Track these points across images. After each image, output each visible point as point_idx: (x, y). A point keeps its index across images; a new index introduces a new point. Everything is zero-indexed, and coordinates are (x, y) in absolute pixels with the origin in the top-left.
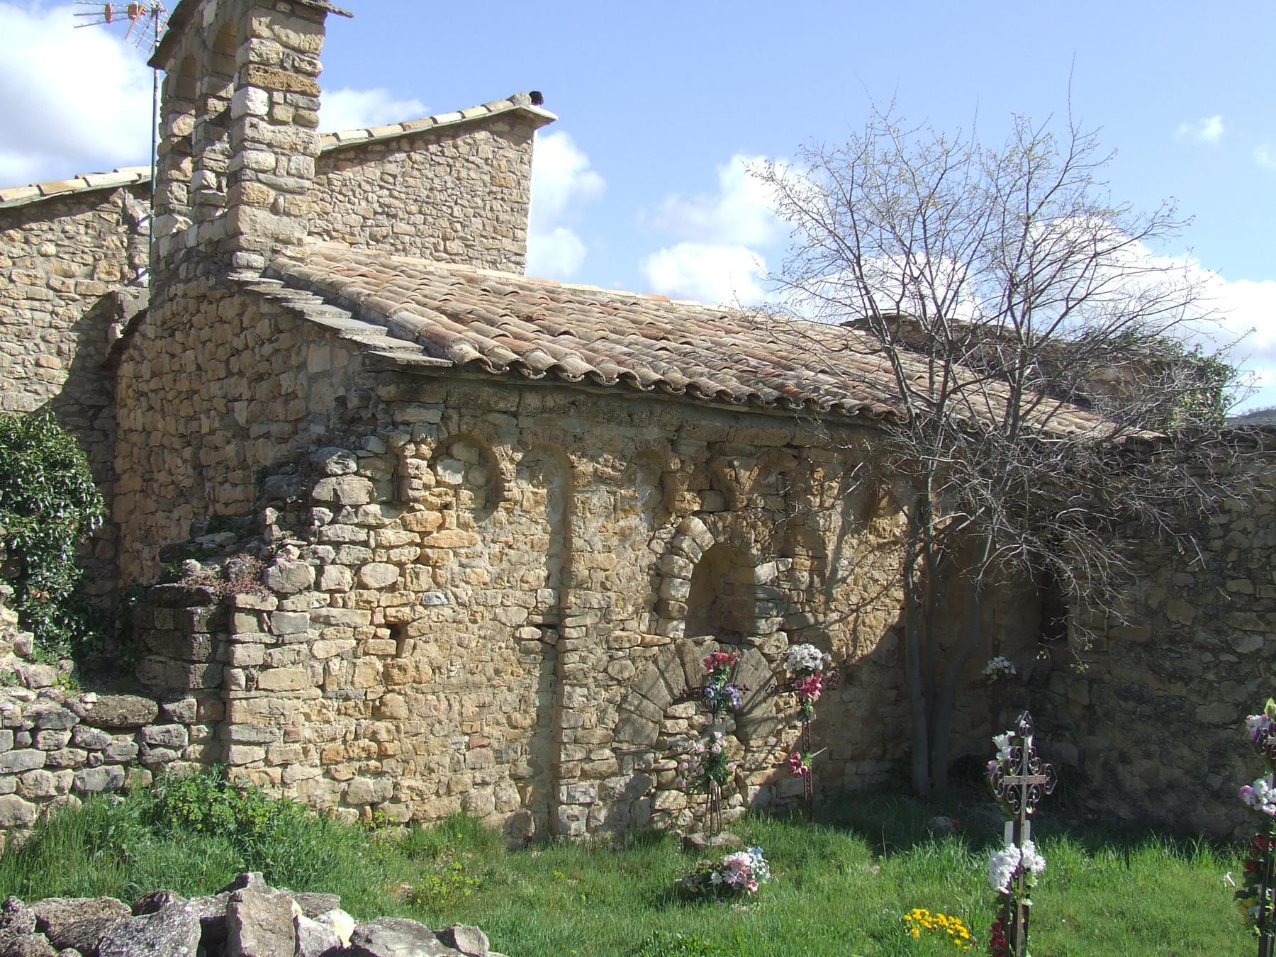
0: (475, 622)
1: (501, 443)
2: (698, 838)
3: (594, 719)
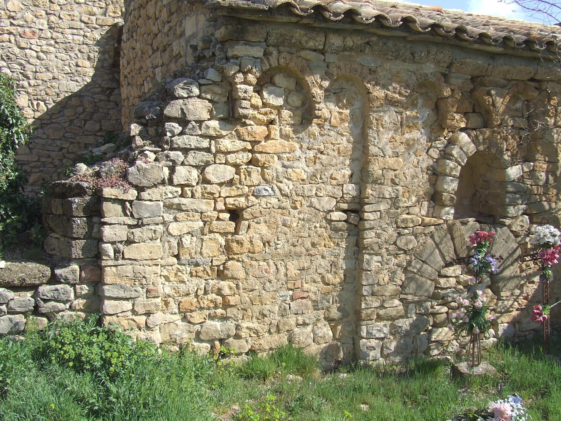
0: (295, 208)
1: (312, 74)
2: (463, 367)
3: (387, 279)
